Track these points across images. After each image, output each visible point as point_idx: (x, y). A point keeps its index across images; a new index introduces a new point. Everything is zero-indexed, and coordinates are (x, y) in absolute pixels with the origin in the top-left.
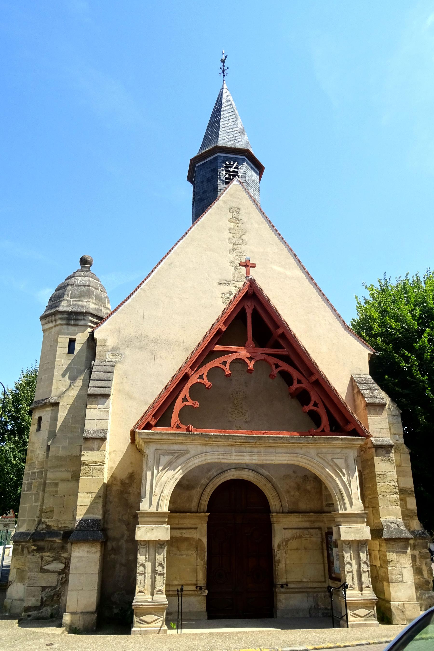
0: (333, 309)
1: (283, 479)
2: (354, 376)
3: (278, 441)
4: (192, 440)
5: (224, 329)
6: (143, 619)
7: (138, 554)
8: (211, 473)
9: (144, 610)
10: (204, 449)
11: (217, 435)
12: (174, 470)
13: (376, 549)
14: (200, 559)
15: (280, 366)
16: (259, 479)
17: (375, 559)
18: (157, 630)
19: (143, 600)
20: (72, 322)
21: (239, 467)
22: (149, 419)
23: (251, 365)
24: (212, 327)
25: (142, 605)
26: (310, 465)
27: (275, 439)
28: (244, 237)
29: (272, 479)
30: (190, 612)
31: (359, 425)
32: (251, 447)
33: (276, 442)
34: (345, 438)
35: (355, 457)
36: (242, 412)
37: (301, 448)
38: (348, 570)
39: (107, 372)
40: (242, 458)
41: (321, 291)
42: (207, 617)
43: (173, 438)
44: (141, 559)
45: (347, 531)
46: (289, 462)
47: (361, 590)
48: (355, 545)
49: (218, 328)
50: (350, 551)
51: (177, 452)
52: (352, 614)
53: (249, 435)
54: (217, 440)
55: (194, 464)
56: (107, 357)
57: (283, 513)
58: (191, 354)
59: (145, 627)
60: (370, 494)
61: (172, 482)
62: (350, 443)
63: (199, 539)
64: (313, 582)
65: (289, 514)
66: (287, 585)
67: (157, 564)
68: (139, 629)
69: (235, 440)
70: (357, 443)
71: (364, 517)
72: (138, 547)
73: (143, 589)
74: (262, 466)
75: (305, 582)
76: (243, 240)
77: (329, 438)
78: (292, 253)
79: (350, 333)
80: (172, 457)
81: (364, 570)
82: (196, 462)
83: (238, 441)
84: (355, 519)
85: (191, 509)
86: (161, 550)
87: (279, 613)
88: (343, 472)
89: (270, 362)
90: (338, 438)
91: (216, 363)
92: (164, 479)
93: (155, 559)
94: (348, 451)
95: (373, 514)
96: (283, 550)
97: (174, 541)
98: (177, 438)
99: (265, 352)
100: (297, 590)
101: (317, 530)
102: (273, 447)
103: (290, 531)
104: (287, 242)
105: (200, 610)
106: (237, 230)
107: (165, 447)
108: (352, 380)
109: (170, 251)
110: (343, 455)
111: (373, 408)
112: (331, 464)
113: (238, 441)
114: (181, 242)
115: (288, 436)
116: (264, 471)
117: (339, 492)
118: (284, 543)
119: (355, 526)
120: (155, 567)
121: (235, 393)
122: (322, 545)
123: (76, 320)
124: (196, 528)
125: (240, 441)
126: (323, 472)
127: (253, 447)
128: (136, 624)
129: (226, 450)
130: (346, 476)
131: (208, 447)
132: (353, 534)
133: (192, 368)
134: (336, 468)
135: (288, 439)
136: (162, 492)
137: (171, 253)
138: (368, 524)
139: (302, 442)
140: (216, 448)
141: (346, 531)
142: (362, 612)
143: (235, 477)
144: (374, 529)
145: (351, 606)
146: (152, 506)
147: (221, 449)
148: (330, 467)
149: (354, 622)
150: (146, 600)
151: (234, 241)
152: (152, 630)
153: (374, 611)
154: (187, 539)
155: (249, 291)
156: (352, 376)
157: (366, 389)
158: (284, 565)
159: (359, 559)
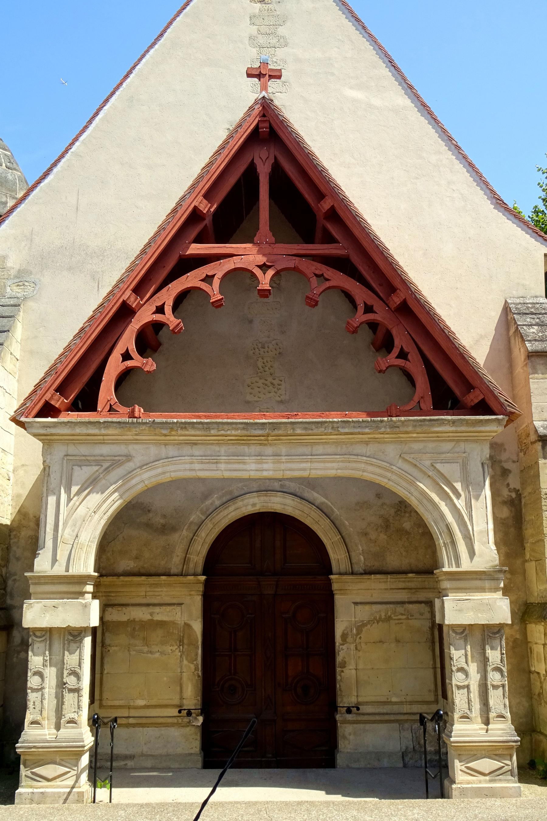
0: (471, 166)
1: (355, 510)
2: (510, 301)
3: (315, 431)
4: (136, 435)
5: (205, 207)
6: (38, 772)
7: (30, 653)
8: (210, 501)
9: (39, 755)
10: (164, 451)
11: (185, 423)
12: (102, 493)
13: (539, 641)
14: (186, 659)
16: (306, 510)
17: (537, 660)
18: (64, 793)
19: (38, 738)
21: (265, 487)
22: (47, 397)
23: (265, 280)
24: (179, 204)
25: (35, 747)
26: (385, 477)
27: (307, 426)
28: (281, 31)
29: (332, 510)
30: (168, 755)
31: (492, 392)
32: (261, 444)
33: (310, 432)
35: (484, 458)
36: (272, 384)
37: (367, 443)
38: (459, 684)
39: (3, 317)
40: (241, 466)
41: (444, 131)
42: (200, 765)
43: (96, 431)
44: (35, 661)
45: (458, 608)
46: (340, 473)
47: (487, 722)
48: (478, 635)
49: (192, 206)
51: (108, 458)
52: (463, 768)
53: (252, 421)
54: (187, 433)
55: (143, 481)
56: (8, 289)
57: (352, 573)
58: (134, 262)
59: (42, 787)
60: (532, 536)
61: (97, 516)
62: (471, 429)
63: (185, 623)
64: (411, 703)
65: (366, 577)
66: (358, 709)
67: (65, 673)
68: (30, 790)
69: (222, 432)
70: (488, 428)
71: (498, 579)
72: (30, 640)
73: (39, 718)
74: (311, 483)
75: (396, 703)
76: (280, 38)
77: (425, 420)
78: (383, 56)
79: (506, 213)
80: (97, 468)
81: (495, 683)
82: (145, 479)
83: (229, 432)
84: (478, 583)
85: (170, 569)
86: (73, 646)
87: (340, 760)
88: (457, 490)
89: (307, 271)
90: (445, 420)
91: (192, 279)
92: (82, 511)
93: (64, 664)
94: (469, 447)
95: (537, 574)
96: (353, 643)
97: (137, 628)
98: (103, 431)
99: (295, 252)
100: (378, 718)
101: (423, 605)
102: (306, 444)
103: (367, 607)
104: (372, 33)
105: (187, 752)
106: (266, 18)
107: (83, 450)
108: (506, 309)
109: (130, 72)
110: (456, 455)
111: (541, 362)
112: (430, 474)
113: (229, 432)
114: (152, 51)
115: (335, 420)
116: (316, 495)
117: (446, 530)
118: (355, 631)
119: (477, 596)
120: (62, 678)
121: (260, 345)
122: (433, 634)
124: (180, 604)
125: (234, 432)
126: (412, 490)
127: (265, 445)
128: (24, 781)
129: (209, 453)
131: (170, 448)
132: (472, 613)
133: (138, 290)
134: (440, 481)
135: (335, 425)
136: (77, 536)
137: (132, 76)
138: (506, 592)
139: (367, 430)
140: (187, 450)
141: (456, 608)
142: (486, 764)
143: (258, 508)
144: (538, 603)
146: (57, 563)
147: (197, 451)
149: (468, 783)
150: (44, 737)
151: (262, 40)
152: (54, 793)
153: (512, 764)
154: (162, 624)
155: (261, 125)
156: (506, 301)
157: (531, 325)
158: (354, 672)
159: (484, 661)
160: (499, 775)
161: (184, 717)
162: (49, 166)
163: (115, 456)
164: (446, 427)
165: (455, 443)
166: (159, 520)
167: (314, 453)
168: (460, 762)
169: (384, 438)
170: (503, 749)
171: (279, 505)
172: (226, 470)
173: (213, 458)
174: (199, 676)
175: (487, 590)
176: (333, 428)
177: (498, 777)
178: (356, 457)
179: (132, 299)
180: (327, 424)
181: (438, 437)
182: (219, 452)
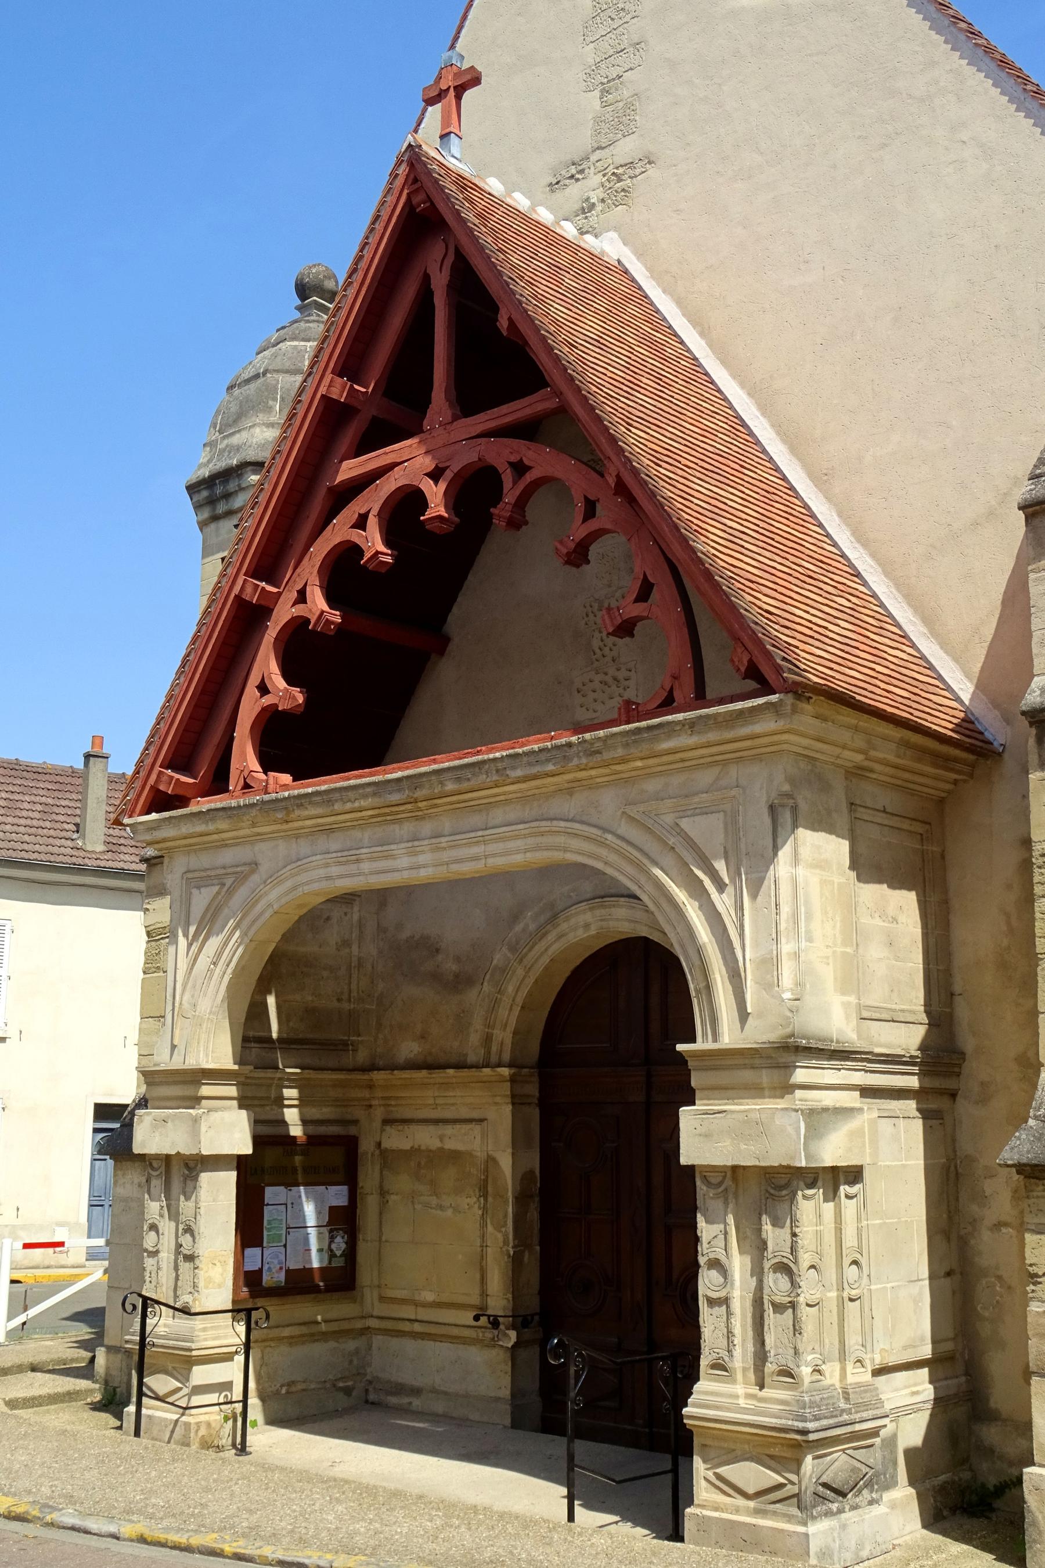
15: (530, 468)
18: (171, 1420)
20: (221, 508)
34: (700, 717)
36: (615, 679)
38: (714, 1295)
42: (508, 1421)
43: (201, 828)
50: (726, 1215)
52: (710, 1474)
54: (306, 813)
55: (270, 905)
70: (758, 728)
77: (639, 730)
81: (778, 1299)
83: (357, 804)
84: (747, 1076)
85: (466, 1055)
105: (493, 1395)
112: (672, 841)
121: (596, 606)
123: (227, 496)
124: (481, 1121)
126: (643, 880)
130: (730, 889)
139: (550, 767)
140: (322, 843)
145: (709, 1442)
147: (335, 843)
148: (669, 860)
149: (716, 1509)
155: (415, 200)
160: (774, 1503)
161: (485, 1328)
162: (458, 22)
163: (237, 866)
164: (680, 738)
165: (720, 767)
166: (451, 967)
167: (490, 825)
168: (704, 1462)
169: (591, 778)
170: (782, 1445)
171: (626, 924)
172: (371, 873)
173: (351, 852)
174: (509, 1256)
175: (767, 1093)
176: (497, 771)
177: (772, 1506)
178: (548, 823)
179: (249, 590)
180: (487, 766)
181: (683, 760)
182: (361, 840)
